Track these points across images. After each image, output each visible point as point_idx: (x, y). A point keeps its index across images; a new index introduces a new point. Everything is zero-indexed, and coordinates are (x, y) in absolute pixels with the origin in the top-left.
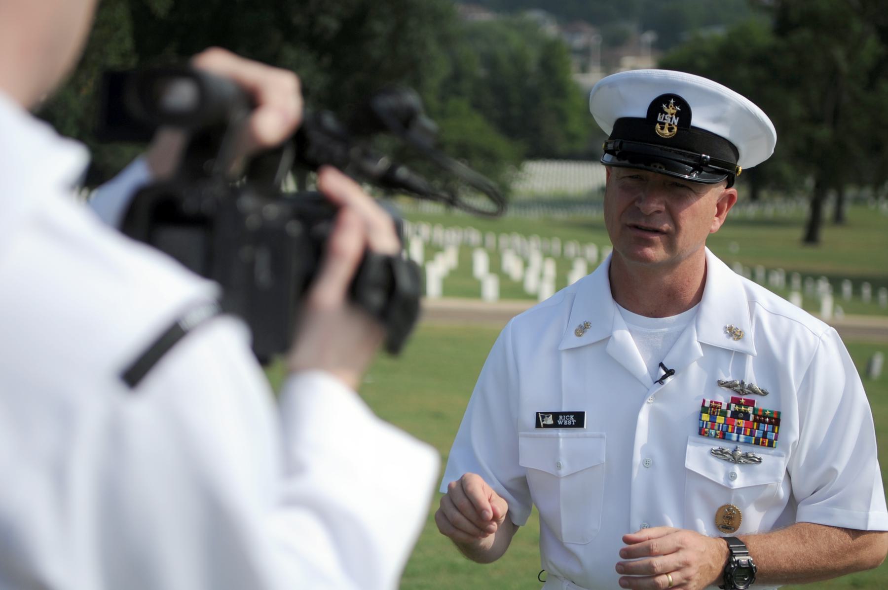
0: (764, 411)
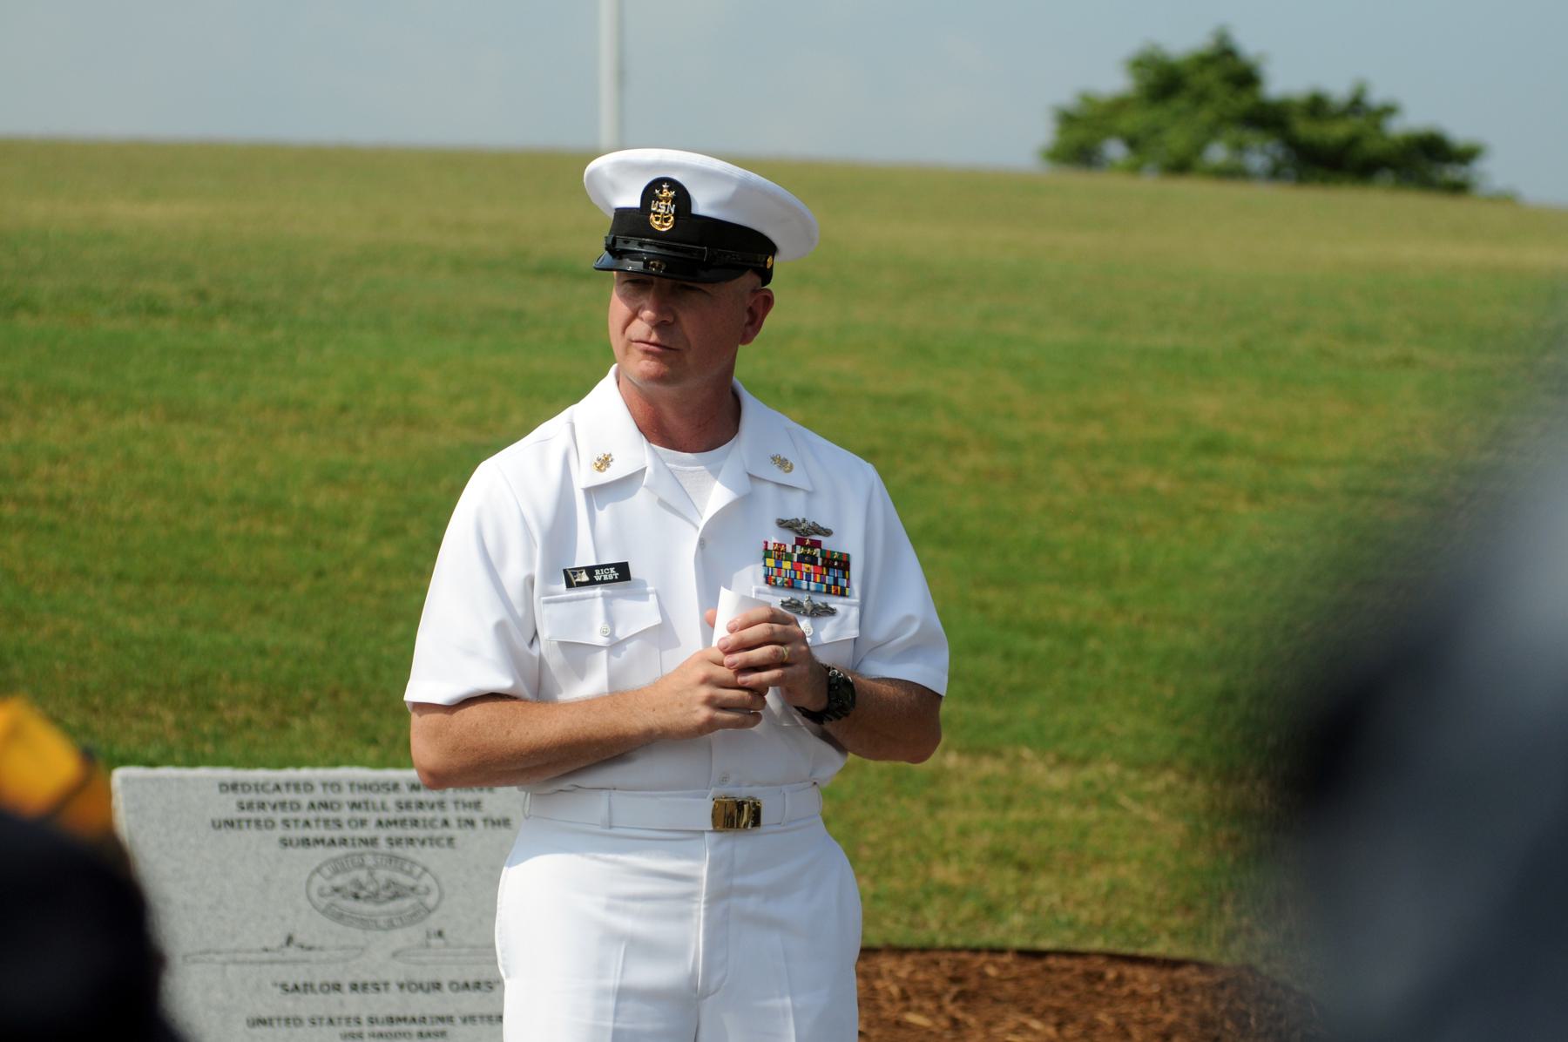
0: (832, 553)
